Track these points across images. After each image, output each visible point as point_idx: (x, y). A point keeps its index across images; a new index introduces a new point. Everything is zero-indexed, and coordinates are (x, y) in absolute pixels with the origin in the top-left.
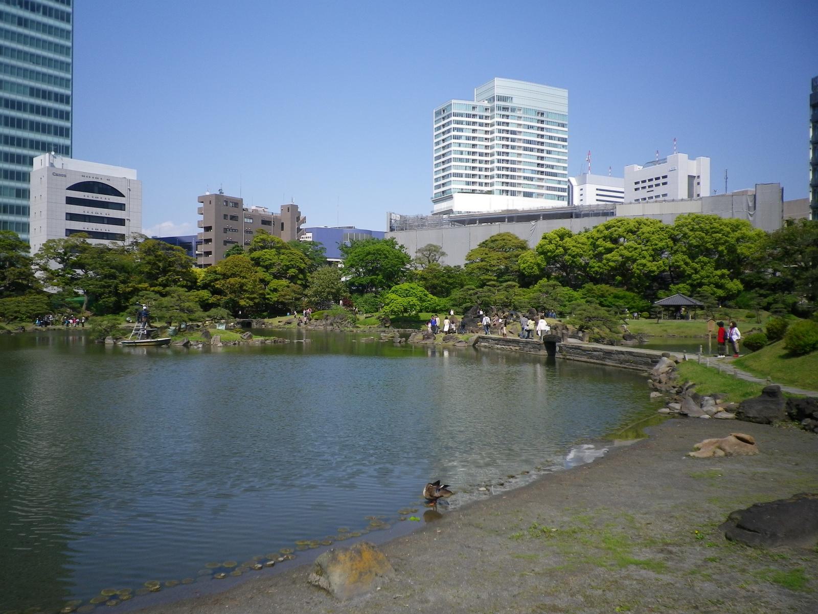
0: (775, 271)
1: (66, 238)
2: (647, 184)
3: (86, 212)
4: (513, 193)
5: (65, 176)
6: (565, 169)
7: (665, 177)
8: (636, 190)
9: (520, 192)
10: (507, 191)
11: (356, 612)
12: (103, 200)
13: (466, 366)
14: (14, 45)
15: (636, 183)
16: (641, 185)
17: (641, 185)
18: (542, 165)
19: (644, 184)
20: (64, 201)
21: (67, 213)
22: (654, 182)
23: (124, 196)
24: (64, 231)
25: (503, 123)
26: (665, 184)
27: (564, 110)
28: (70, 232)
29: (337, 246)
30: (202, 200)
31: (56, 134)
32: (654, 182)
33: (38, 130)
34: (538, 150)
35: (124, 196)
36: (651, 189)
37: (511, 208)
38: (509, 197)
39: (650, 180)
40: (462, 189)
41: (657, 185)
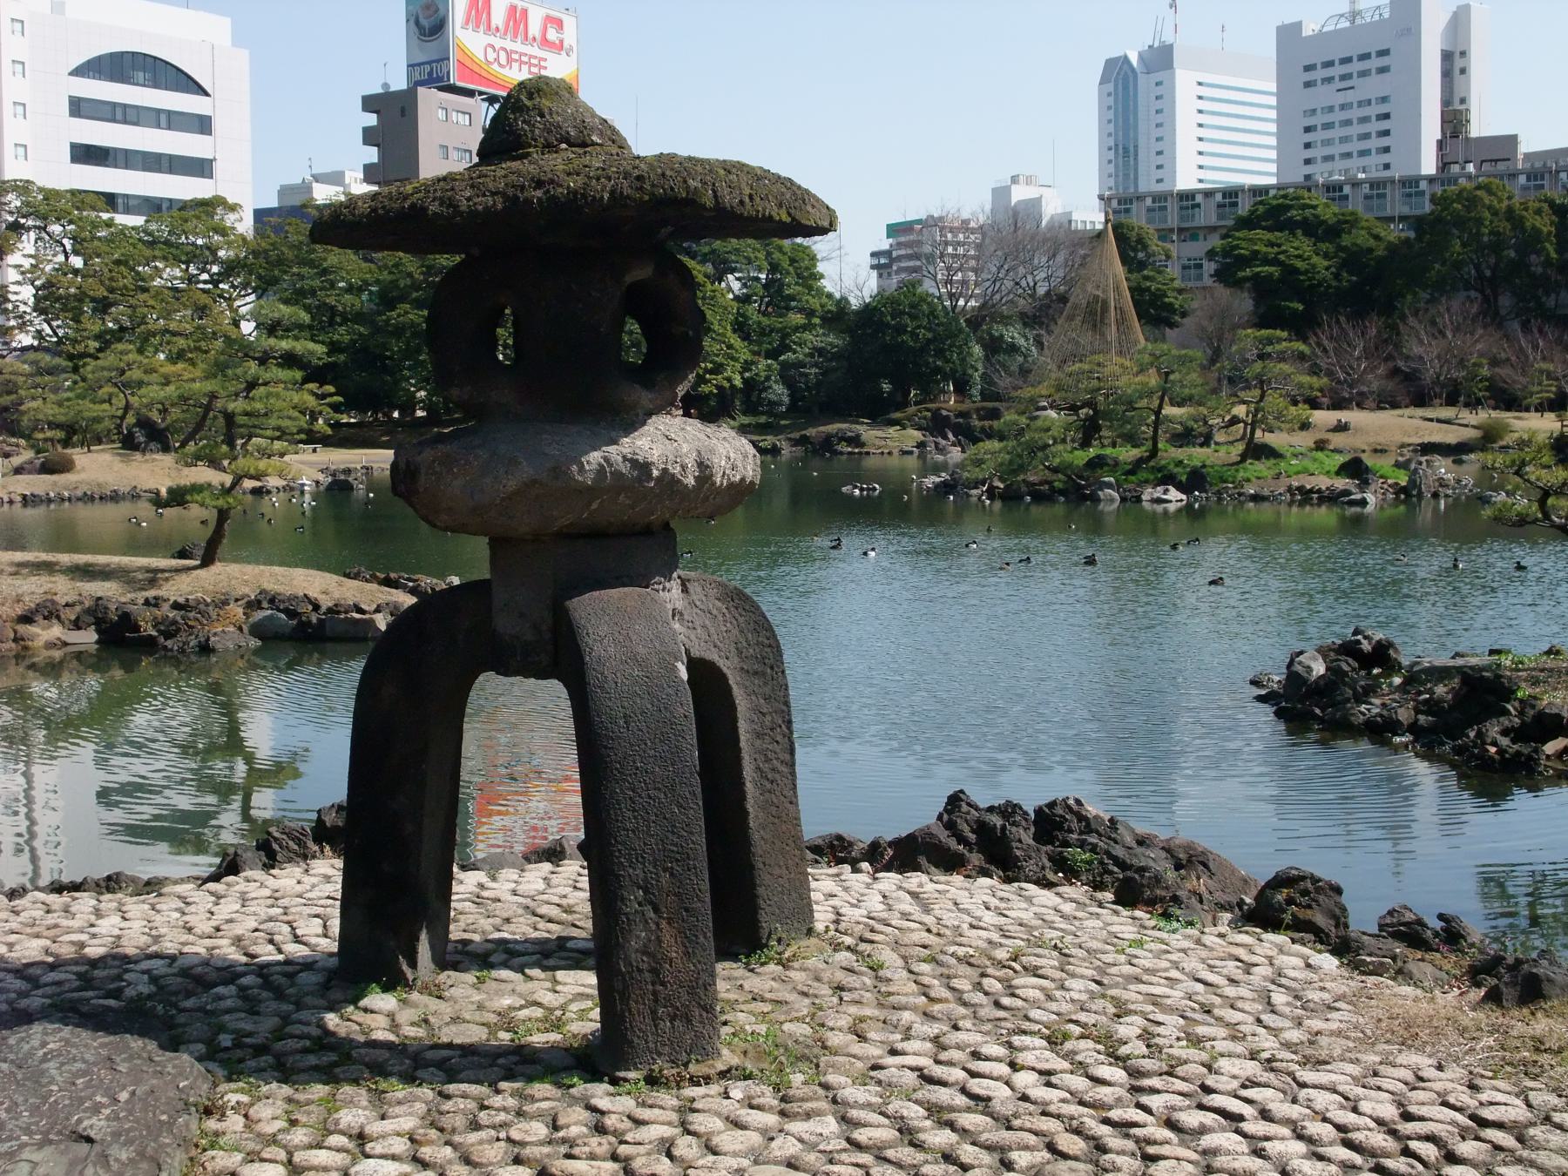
5: (13, 20)
7: (1384, 53)
8: (1308, 85)
9: (481, 93)
11: (5, 1066)
13: (187, 600)
16: (1320, 74)
17: (1320, 74)
19: (1329, 72)
22: (1356, 66)
23: (206, 94)
26: (1383, 70)
29: (886, 965)
32: (1356, 66)
35: (206, 94)
41: (1364, 74)
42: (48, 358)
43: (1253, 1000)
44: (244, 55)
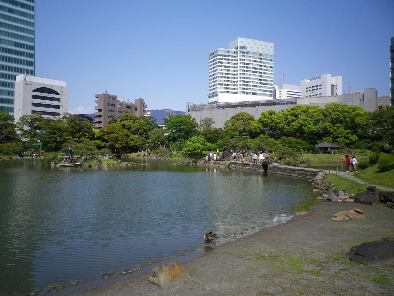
0: (374, 130)
1: (32, 115)
2: (312, 89)
3: (41, 102)
4: (247, 93)
5: (31, 85)
7: (320, 85)
8: (306, 91)
9: (250, 93)
10: (244, 92)
12: (50, 96)
14: (7, 22)
15: (306, 88)
16: (309, 89)
17: (309, 89)
18: (261, 80)
19: (310, 89)
20: (31, 97)
21: (32, 103)
22: (315, 88)
23: (60, 95)
24: (31, 111)
25: (242, 59)
26: (320, 89)
27: (272, 53)
28: (33, 112)
31: (27, 65)
32: (315, 88)
33: (18, 63)
34: (259, 72)
35: (60, 95)
36: (313, 91)
37: (246, 100)
38: (245, 95)
39: (313, 87)
40: (223, 91)
41: (317, 89)
43: (383, 267)
44: (144, 101)
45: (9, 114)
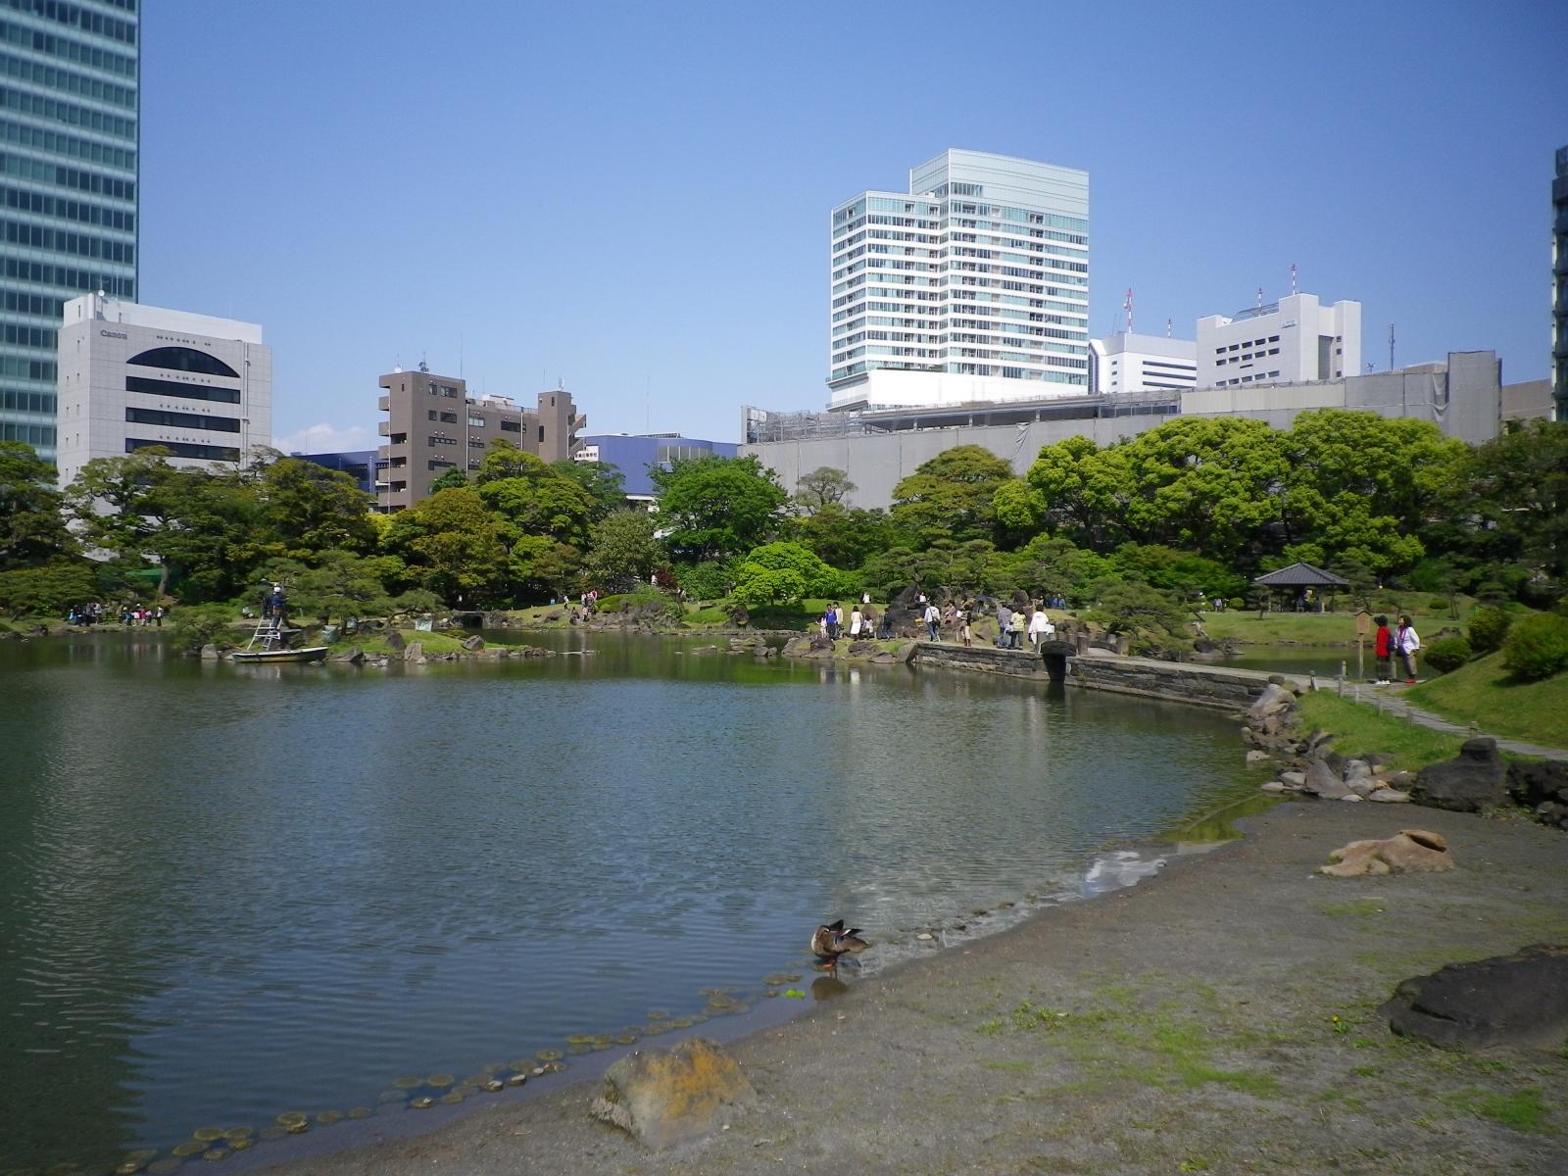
1: (127, 456)
2: (1241, 352)
3: (165, 405)
4: (984, 371)
5: (125, 337)
6: (1082, 323)
7: (1274, 339)
8: (1219, 363)
9: (996, 368)
10: (972, 366)
11: (683, 1173)
12: (198, 383)
15: (1219, 351)
16: (1228, 355)
17: (1228, 355)
18: (1039, 317)
19: (1235, 353)
20: (123, 384)
21: (128, 409)
22: (1254, 349)
23: (238, 376)
24: (123, 443)
25: (965, 235)
26: (1274, 352)
27: (1082, 210)
28: (133, 444)
30: (386, 383)
31: (107, 256)
32: (1254, 349)
33: (72, 249)
34: (1032, 286)
35: (238, 376)
36: (1248, 362)
37: (979, 398)
38: (977, 378)
39: (1246, 345)
40: (886, 362)
41: (1260, 355)
42: (1249, 1100)
45: (38, 452)
